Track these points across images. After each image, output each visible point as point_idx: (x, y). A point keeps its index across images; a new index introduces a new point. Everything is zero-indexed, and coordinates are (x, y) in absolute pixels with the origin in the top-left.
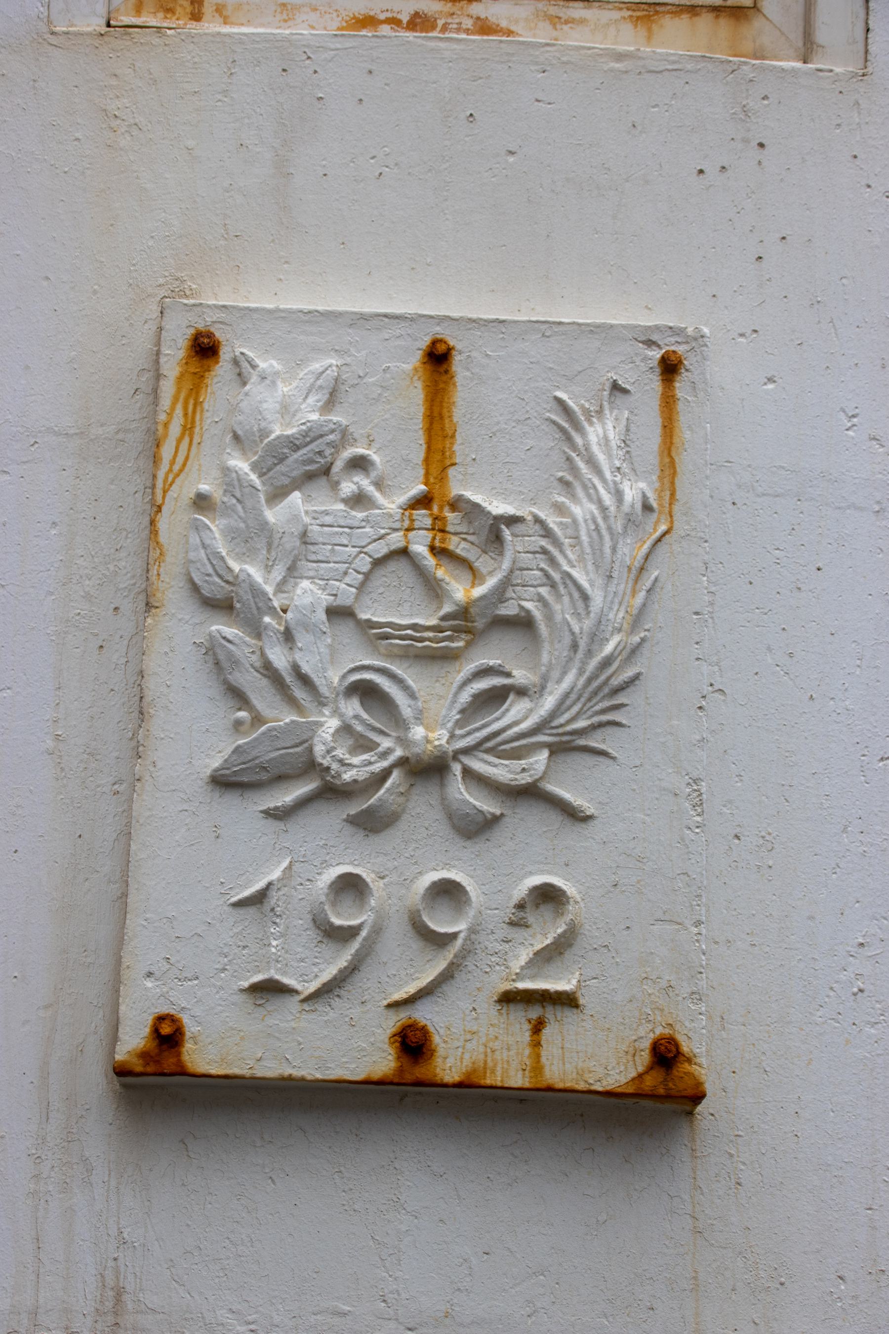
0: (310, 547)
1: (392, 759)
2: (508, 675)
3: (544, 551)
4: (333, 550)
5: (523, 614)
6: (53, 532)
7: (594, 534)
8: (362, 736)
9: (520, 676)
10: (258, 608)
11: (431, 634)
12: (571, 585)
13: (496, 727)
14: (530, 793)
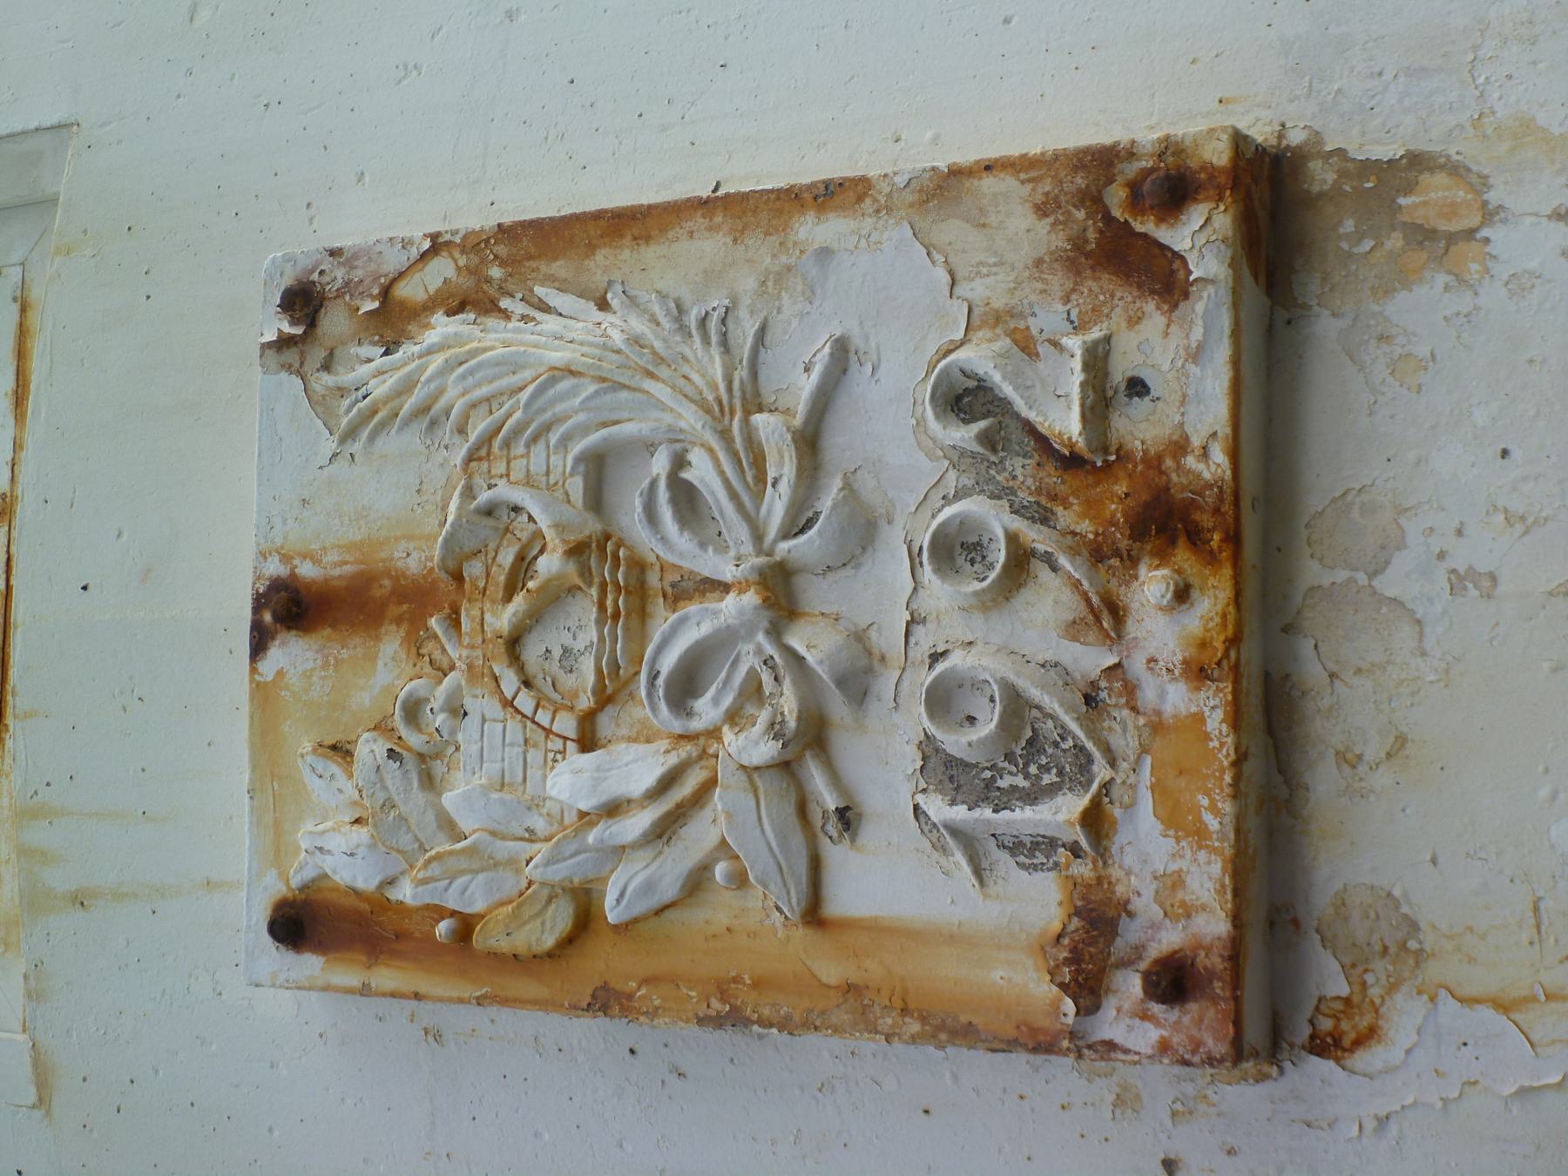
0: (507, 779)
1: (770, 650)
2: (653, 484)
3: (507, 444)
4: (511, 745)
5: (582, 468)
6: (546, 1137)
7: (478, 376)
8: (740, 694)
9: (660, 464)
10: (577, 853)
11: (610, 597)
12: (541, 402)
13: (722, 495)
14: (809, 442)
